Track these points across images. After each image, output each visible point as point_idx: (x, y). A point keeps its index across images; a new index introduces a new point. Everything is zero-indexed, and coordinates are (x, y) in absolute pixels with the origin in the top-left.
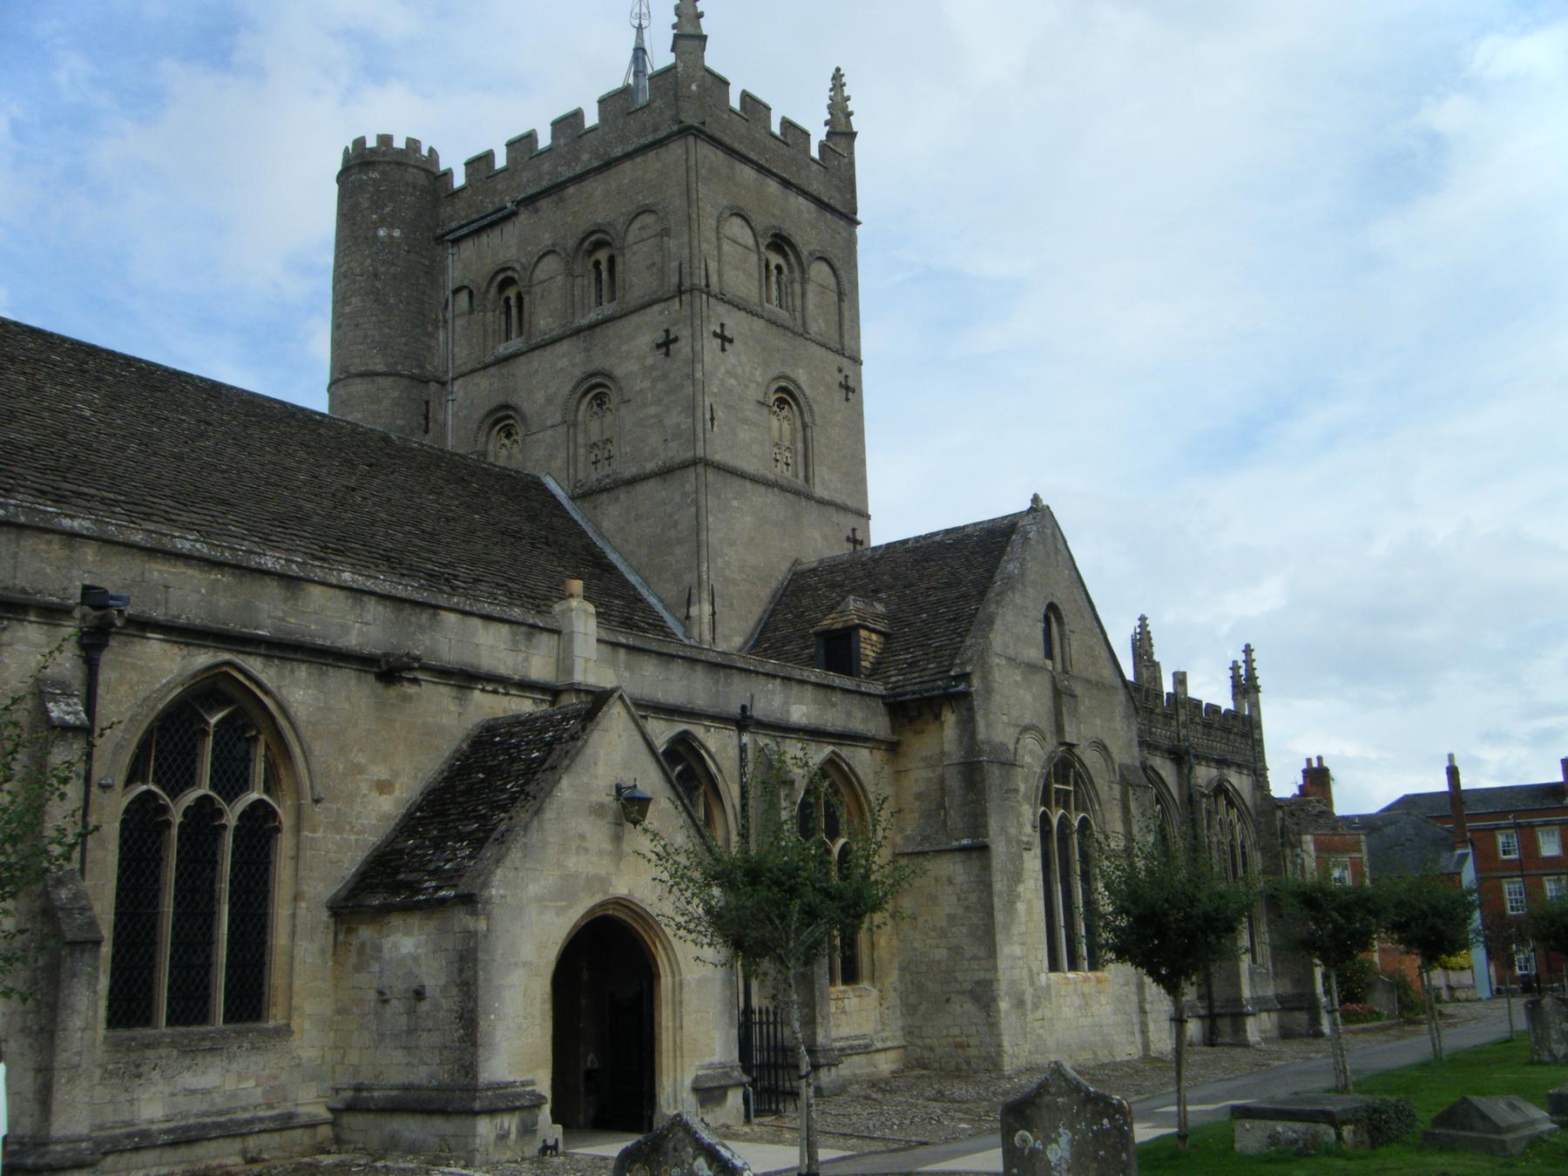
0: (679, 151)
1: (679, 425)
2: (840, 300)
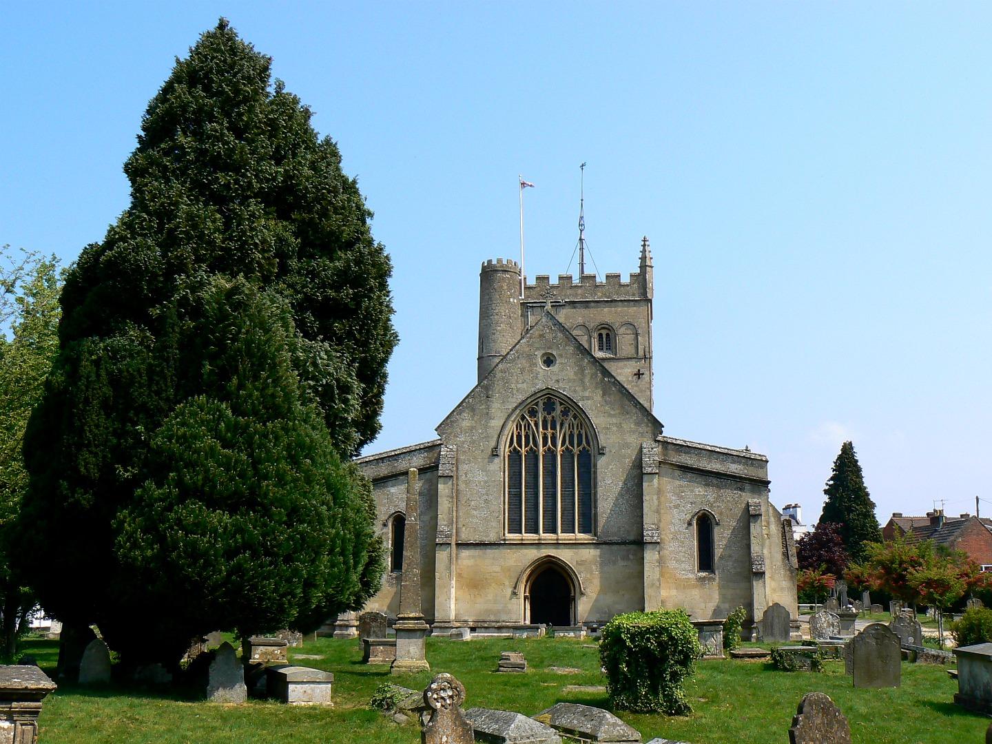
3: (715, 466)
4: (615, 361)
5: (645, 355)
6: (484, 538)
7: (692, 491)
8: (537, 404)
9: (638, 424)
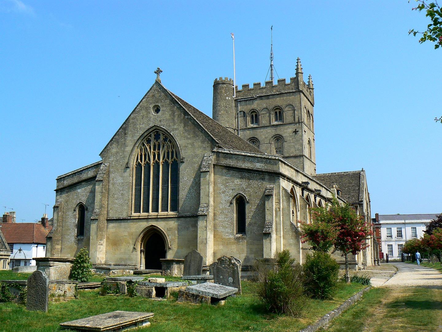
1: (298, 148)
2: (313, 122)
3: (247, 165)
4: (283, 125)
6: (120, 216)
7: (233, 182)
8: (150, 136)
9: (203, 142)
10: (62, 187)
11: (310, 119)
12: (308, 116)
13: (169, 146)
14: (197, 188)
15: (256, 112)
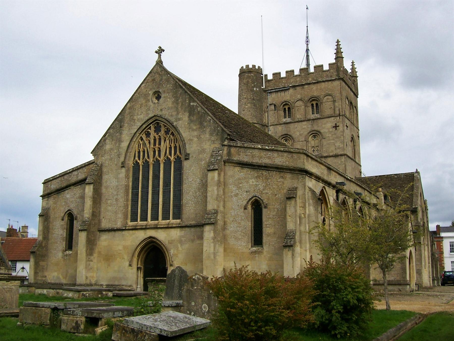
0: (338, 83)
1: (339, 146)
5: (339, 114)
8: (150, 128)
10: (49, 191)
11: (353, 112)
12: (350, 108)
13: (172, 140)
14: (204, 190)
15: (289, 105)
